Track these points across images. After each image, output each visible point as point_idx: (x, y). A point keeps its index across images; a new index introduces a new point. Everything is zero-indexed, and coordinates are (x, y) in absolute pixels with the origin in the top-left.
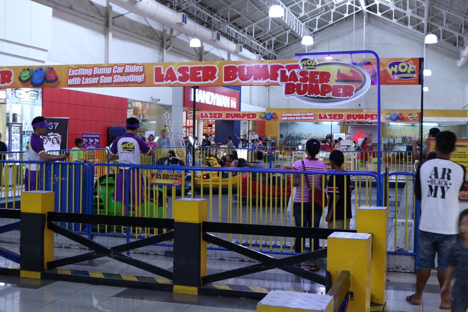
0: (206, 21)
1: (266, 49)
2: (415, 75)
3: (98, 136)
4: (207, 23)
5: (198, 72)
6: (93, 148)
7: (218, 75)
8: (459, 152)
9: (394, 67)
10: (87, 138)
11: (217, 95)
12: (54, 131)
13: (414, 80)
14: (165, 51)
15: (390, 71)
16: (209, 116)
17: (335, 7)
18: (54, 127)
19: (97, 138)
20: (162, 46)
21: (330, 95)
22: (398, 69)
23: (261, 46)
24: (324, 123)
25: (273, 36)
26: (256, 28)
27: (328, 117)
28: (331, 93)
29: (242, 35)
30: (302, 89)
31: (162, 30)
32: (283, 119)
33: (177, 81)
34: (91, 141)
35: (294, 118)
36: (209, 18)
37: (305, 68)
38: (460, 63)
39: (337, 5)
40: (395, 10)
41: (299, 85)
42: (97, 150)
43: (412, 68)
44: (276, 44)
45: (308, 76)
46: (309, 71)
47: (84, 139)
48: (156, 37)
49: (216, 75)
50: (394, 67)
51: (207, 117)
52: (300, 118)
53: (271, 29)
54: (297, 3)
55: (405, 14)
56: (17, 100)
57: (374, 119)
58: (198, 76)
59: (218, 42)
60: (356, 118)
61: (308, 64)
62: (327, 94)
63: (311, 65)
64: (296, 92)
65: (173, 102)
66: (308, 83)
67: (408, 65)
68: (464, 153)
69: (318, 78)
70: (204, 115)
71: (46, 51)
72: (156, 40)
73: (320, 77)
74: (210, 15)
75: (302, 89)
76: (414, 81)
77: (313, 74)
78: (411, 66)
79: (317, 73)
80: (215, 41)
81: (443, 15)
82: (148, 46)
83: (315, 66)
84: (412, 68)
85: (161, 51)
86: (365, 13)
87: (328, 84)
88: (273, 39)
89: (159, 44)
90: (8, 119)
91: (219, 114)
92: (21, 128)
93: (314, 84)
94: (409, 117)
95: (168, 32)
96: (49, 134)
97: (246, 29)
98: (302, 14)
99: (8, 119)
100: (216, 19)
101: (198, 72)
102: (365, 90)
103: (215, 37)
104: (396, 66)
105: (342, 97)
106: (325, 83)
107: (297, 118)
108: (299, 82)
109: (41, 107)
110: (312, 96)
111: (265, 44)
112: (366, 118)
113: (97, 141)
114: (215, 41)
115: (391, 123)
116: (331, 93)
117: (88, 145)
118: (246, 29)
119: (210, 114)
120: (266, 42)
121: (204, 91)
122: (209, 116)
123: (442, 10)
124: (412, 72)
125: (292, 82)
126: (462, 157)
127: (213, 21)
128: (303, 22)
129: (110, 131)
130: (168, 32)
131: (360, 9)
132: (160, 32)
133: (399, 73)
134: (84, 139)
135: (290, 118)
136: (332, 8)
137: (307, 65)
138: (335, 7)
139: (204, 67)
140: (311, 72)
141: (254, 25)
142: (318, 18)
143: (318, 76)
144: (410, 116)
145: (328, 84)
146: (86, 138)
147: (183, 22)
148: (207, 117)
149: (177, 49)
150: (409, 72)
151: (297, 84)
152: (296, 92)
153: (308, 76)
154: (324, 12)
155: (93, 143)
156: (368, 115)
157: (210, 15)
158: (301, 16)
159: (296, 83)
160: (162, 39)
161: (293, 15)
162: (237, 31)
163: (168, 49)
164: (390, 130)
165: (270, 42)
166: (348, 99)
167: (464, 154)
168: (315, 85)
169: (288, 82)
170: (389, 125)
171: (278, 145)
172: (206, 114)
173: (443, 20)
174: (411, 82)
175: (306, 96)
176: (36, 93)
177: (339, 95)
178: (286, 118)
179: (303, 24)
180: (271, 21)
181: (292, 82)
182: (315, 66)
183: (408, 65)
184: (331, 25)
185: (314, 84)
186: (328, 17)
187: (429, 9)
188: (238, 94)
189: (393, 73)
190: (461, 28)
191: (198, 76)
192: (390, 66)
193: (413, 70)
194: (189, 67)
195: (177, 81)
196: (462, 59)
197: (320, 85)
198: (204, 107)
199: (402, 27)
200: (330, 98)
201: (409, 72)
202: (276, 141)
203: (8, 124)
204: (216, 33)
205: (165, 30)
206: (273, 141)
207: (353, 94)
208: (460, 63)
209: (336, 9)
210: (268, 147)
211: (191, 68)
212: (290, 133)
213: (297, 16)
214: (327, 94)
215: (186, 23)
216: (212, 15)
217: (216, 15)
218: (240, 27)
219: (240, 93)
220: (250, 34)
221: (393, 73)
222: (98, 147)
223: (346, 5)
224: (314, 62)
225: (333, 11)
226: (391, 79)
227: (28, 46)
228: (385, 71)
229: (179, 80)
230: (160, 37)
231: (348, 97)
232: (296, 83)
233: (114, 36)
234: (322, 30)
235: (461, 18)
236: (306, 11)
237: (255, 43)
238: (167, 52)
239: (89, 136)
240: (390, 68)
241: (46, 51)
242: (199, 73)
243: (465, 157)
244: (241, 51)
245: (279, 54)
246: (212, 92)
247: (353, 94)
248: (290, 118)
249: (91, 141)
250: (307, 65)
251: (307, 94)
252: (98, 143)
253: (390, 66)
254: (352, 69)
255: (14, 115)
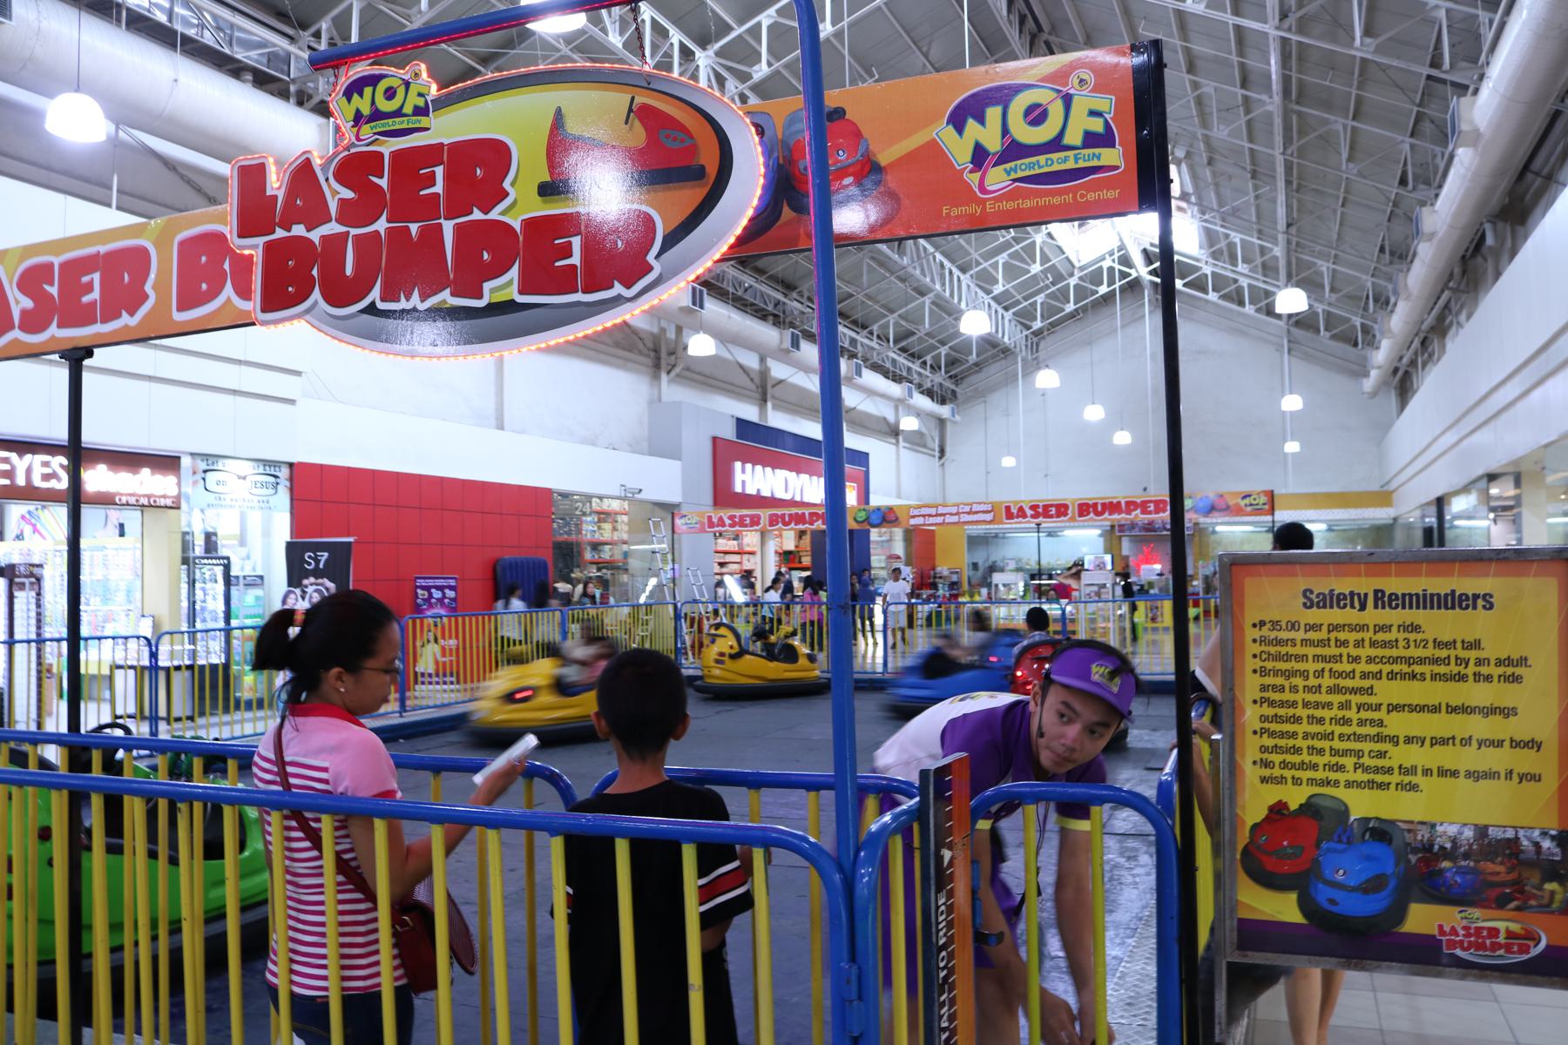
0: (770, 308)
1: (927, 373)
2: (1111, 156)
3: (452, 582)
4: (775, 316)
5: (85, 279)
6: (443, 612)
7: (154, 288)
8: (1438, 644)
9: (981, 120)
10: (428, 588)
11: (804, 477)
12: (317, 573)
13: (1109, 184)
14: (664, 377)
15: (959, 149)
16: (728, 522)
17: (1077, 274)
18: (317, 562)
19: (451, 588)
20: (657, 366)
21: (505, 286)
22: (1005, 131)
23: (916, 367)
24: (1068, 533)
25: (943, 343)
26: (896, 324)
27: (1029, 512)
28: (514, 273)
29: (866, 341)
30: (349, 271)
31: (655, 330)
32: (913, 522)
33: (16, 334)
34: (437, 594)
35: (940, 520)
36: (777, 303)
37: (367, 131)
38: (1369, 384)
39: (1082, 268)
40: (1213, 273)
41: (335, 244)
42: (449, 617)
43: (1093, 113)
44: (952, 362)
45: (383, 183)
46: (388, 147)
47: (420, 591)
48: (641, 346)
49: (148, 288)
50: (981, 120)
51: (723, 525)
52: (955, 519)
53: (931, 324)
54: (985, 265)
55: (1236, 281)
56: (210, 498)
57: (91, 283)
58: (86, 299)
59: (858, 380)
60: (1101, 513)
61: (385, 106)
62: (487, 286)
63: (398, 113)
64: (316, 294)
65: (684, 493)
66: (381, 225)
67: (1068, 100)
68: (1476, 645)
69: (439, 188)
70: (715, 520)
71: (298, 373)
72: (640, 353)
73: (448, 177)
74: (780, 297)
75: (349, 271)
76: (1112, 194)
77: (411, 165)
78: (1081, 105)
79: (432, 154)
80: (788, 351)
81: (1322, 274)
82: (618, 367)
83: (421, 111)
84: (1093, 113)
85: (656, 377)
86: (1146, 284)
87: (494, 215)
88: (944, 350)
89: (648, 361)
90: (186, 545)
91: (752, 517)
92: (227, 568)
93: (414, 228)
94: (1242, 503)
95: (671, 335)
96: (306, 582)
97: (875, 328)
98: (999, 289)
99: (186, 545)
100: (795, 304)
101: (85, 279)
102: (721, 237)
103: (787, 344)
104: (993, 113)
105: (579, 297)
106: (477, 215)
107: (949, 519)
108: (333, 228)
109: (288, 516)
110: (403, 304)
111: (925, 363)
112: (1129, 512)
113: (450, 594)
114: (788, 351)
115: (1218, 528)
116: (514, 273)
117: (431, 606)
118: (875, 328)
119: (731, 518)
120: (928, 358)
121: (768, 469)
122: (728, 522)
123: (1320, 262)
124: (1091, 140)
125: (298, 230)
126: (1462, 678)
127: (788, 309)
128: (1006, 309)
129: (499, 568)
130: (671, 335)
131: (1134, 275)
132: (652, 334)
133: (1014, 151)
134: (420, 591)
135: (932, 520)
136: (1072, 275)
137: (377, 115)
138: (1077, 274)
139: (109, 254)
140: (397, 155)
141: (892, 319)
142: (1040, 299)
143: (439, 171)
144: (1247, 501)
145: (494, 215)
146: (423, 588)
147: (694, 303)
148: (723, 525)
149: (699, 374)
150: (1074, 137)
151: (324, 238)
152: (316, 294)
153: (383, 183)
154: (1053, 284)
155: (441, 601)
156: (1133, 503)
157: (780, 297)
158: (996, 292)
159: (315, 236)
160: (656, 351)
161: (981, 294)
162: (853, 335)
163: (673, 374)
164: (1219, 543)
165: (937, 358)
166: (618, 300)
167: (1473, 655)
168: (422, 230)
169: (280, 233)
170: (1214, 532)
171: (965, 586)
172: (721, 519)
173: (1323, 287)
174: (1091, 196)
175: (371, 310)
176: (272, 479)
177: (565, 281)
178: (920, 521)
179: (1008, 315)
180: (931, 311)
181: (298, 230)
182: (421, 111)
183: (1068, 100)
184: (1072, 315)
185: (414, 228)
186: (1063, 295)
187: (1289, 264)
188: (862, 475)
189: (980, 156)
190: (1367, 303)
191: (86, 299)
192: (957, 122)
193: (1097, 126)
194: (57, 261)
195: (16, 334)
196: (1374, 373)
197: (448, 227)
198: (759, 501)
199: (1231, 310)
200: (509, 306)
201: (1074, 137)
202: (960, 578)
203: (185, 561)
204: (788, 333)
205: (663, 330)
206: (955, 578)
207: (650, 269)
208: (1369, 384)
209: (1081, 278)
210: (941, 592)
211: (63, 266)
212: (992, 559)
213: (988, 292)
214: (487, 286)
215: (702, 307)
216: (786, 295)
217: (794, 295)
218: (864, 327)
219: (867, 474)
220: (882, 338)
221: (980, 156)
222: (455, 610)
223: (1101, 268)
224: (414, 90)
225: (1073, 281)
226: (963, 194)
227: (240, 362)
228: (933, 151)
229: (22, 328)
230: (650, 345)
231: (618, 289)
232: (315, 236)
233: (774, 408)
234: (1053, 325)
235: (1364, 277)
236: (1008, 278)
237: (902, 360)
238: (669, 382)
239: (431, 582)
240: (960, 129)
241: (298, 373)
242: (89, 288)
243: (1477, 677)
244: (859, 374)
245: (964, 385)
246: (791, 470)
247: (650, 269)
248: (932, 520)
249: (437, 594)
250: (377, 115)
251: (375, 294)
252: (454, 600)
253: (957, 122)
254: (639, 100)
255: (210, 538)
